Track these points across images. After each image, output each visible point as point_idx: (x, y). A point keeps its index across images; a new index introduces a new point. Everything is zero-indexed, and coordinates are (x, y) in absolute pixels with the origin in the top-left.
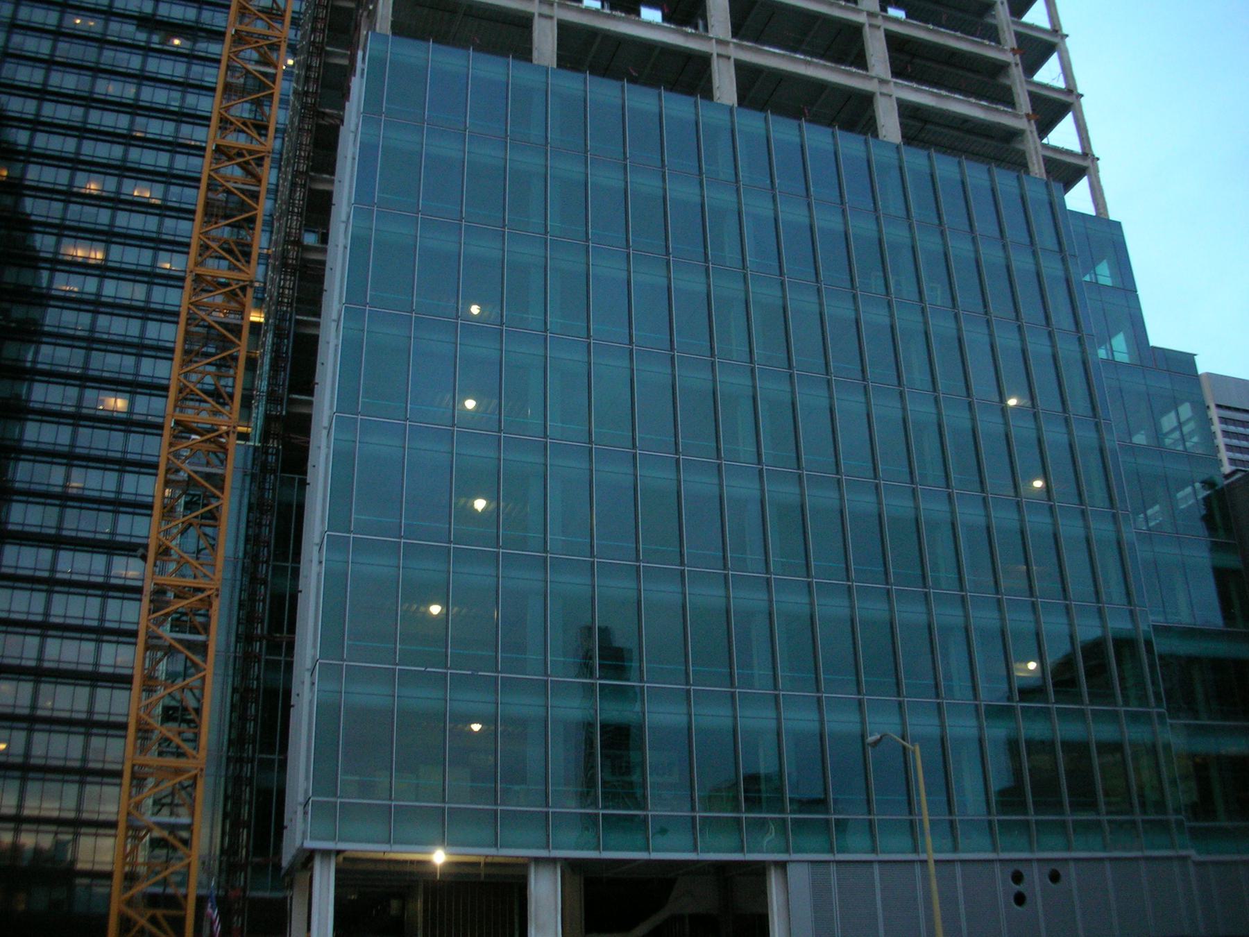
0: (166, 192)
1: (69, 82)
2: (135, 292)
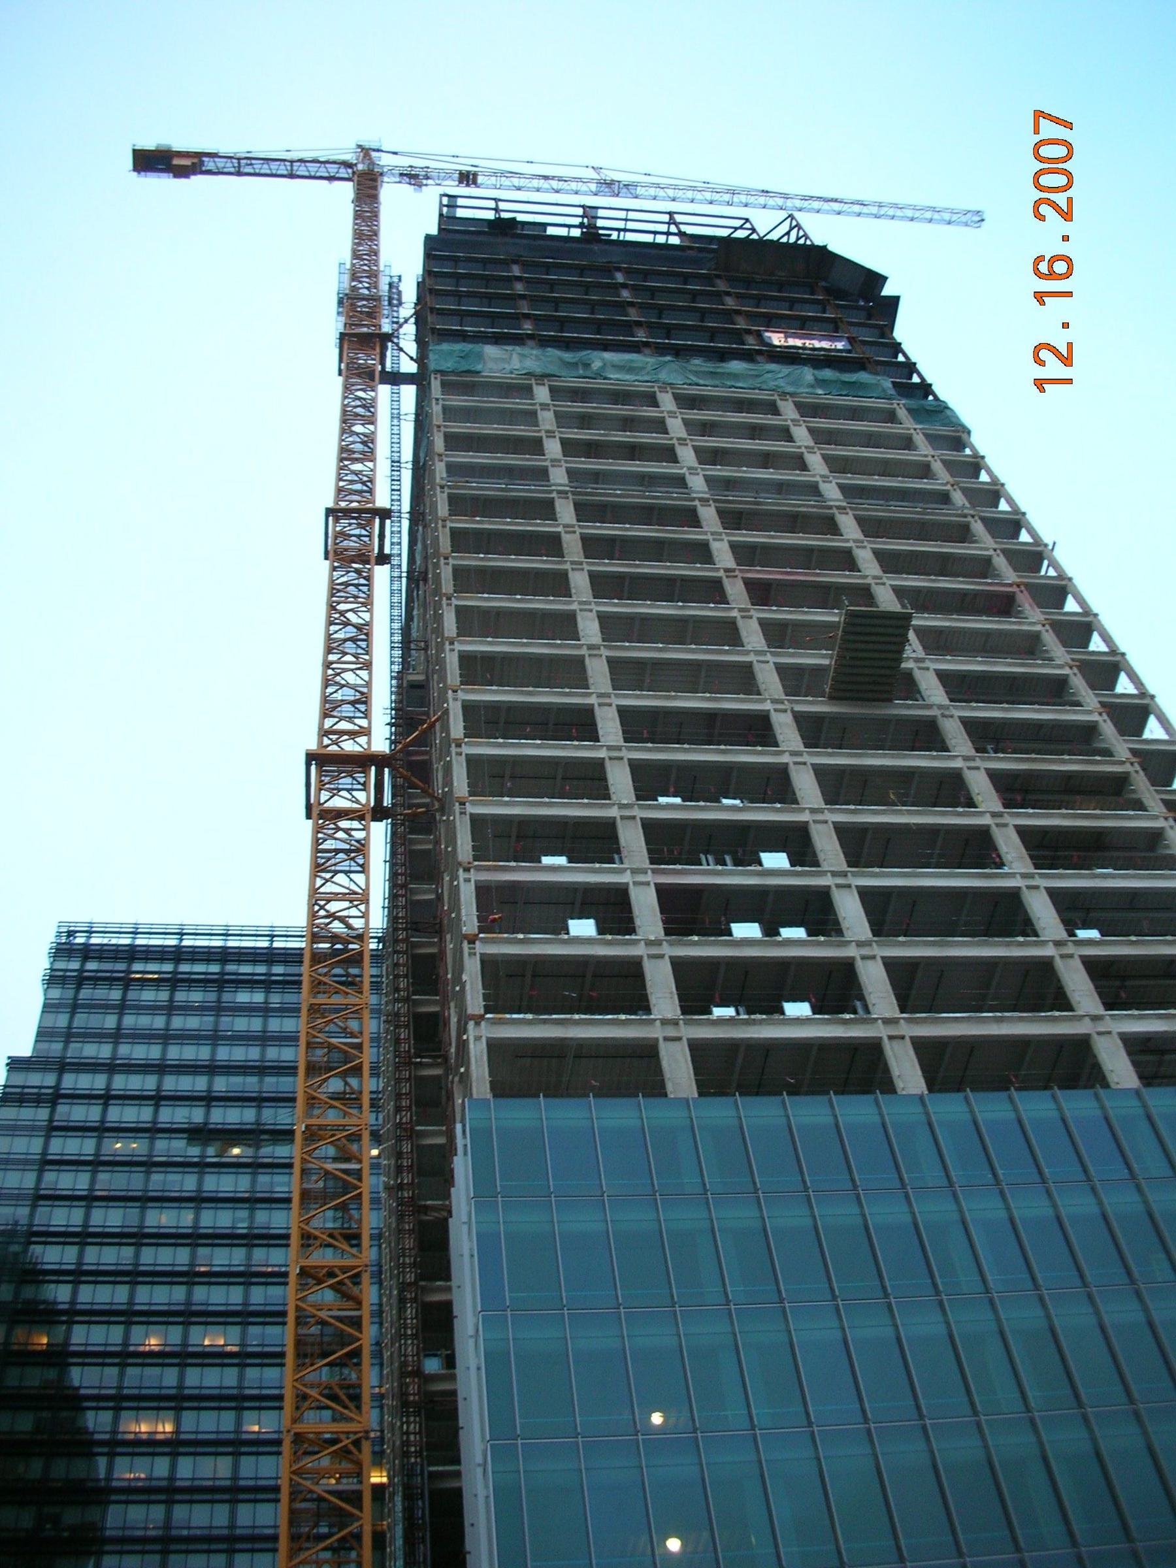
0: (244, 1335)
1: (112, 1218)
2: (218, 1469)
